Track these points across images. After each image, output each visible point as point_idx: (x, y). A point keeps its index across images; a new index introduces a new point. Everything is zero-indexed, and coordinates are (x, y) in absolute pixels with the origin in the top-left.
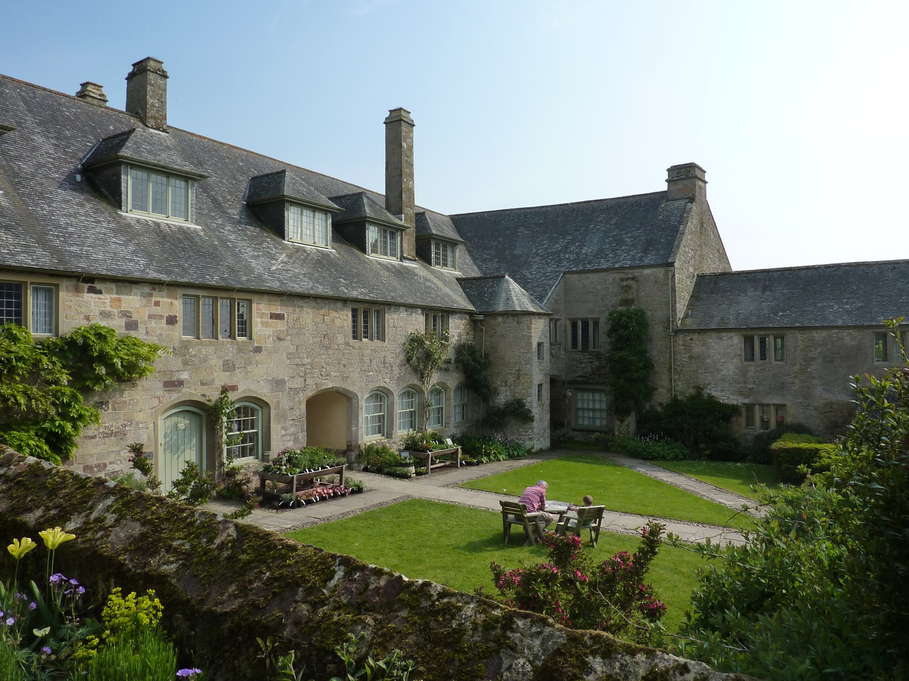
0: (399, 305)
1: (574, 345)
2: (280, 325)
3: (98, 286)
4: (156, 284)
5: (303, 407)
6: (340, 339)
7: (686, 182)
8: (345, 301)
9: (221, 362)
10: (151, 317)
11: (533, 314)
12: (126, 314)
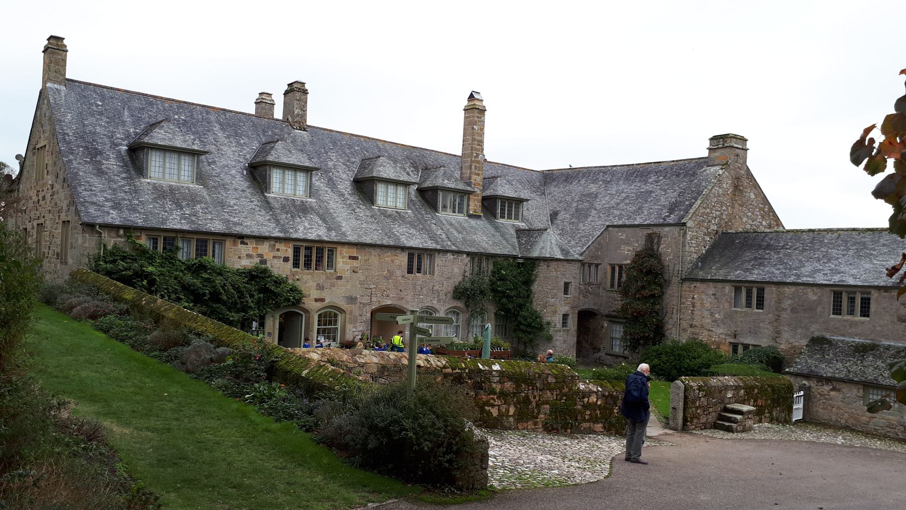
0: (445, 251)
1: (612, 286)
2: (355, 263)
3: (246, 241)
4: (277, 239)
5: (369, 315)
6: (398, 273)
7: (723, 151)
8: (403, 248)
9: (315, 284)
10: (274, 257)
11: (560, 260)
12: (261, 256)
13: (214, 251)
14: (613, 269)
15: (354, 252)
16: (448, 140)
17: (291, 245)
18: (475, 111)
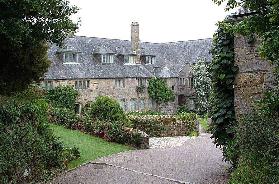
1: (190, 86)
3: (59, 81)
4: (70, 79)
11: (170, 78)
13: (110, 61)
14: (189, 79)
15: (96, 81)
16: (127, 36)
17: (74, 81)
18: (135, 26)
